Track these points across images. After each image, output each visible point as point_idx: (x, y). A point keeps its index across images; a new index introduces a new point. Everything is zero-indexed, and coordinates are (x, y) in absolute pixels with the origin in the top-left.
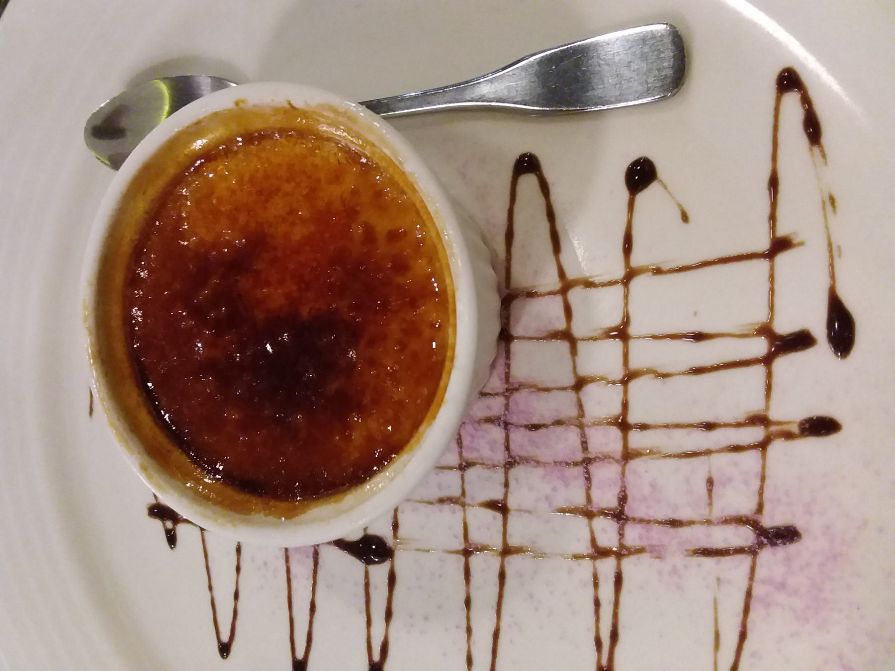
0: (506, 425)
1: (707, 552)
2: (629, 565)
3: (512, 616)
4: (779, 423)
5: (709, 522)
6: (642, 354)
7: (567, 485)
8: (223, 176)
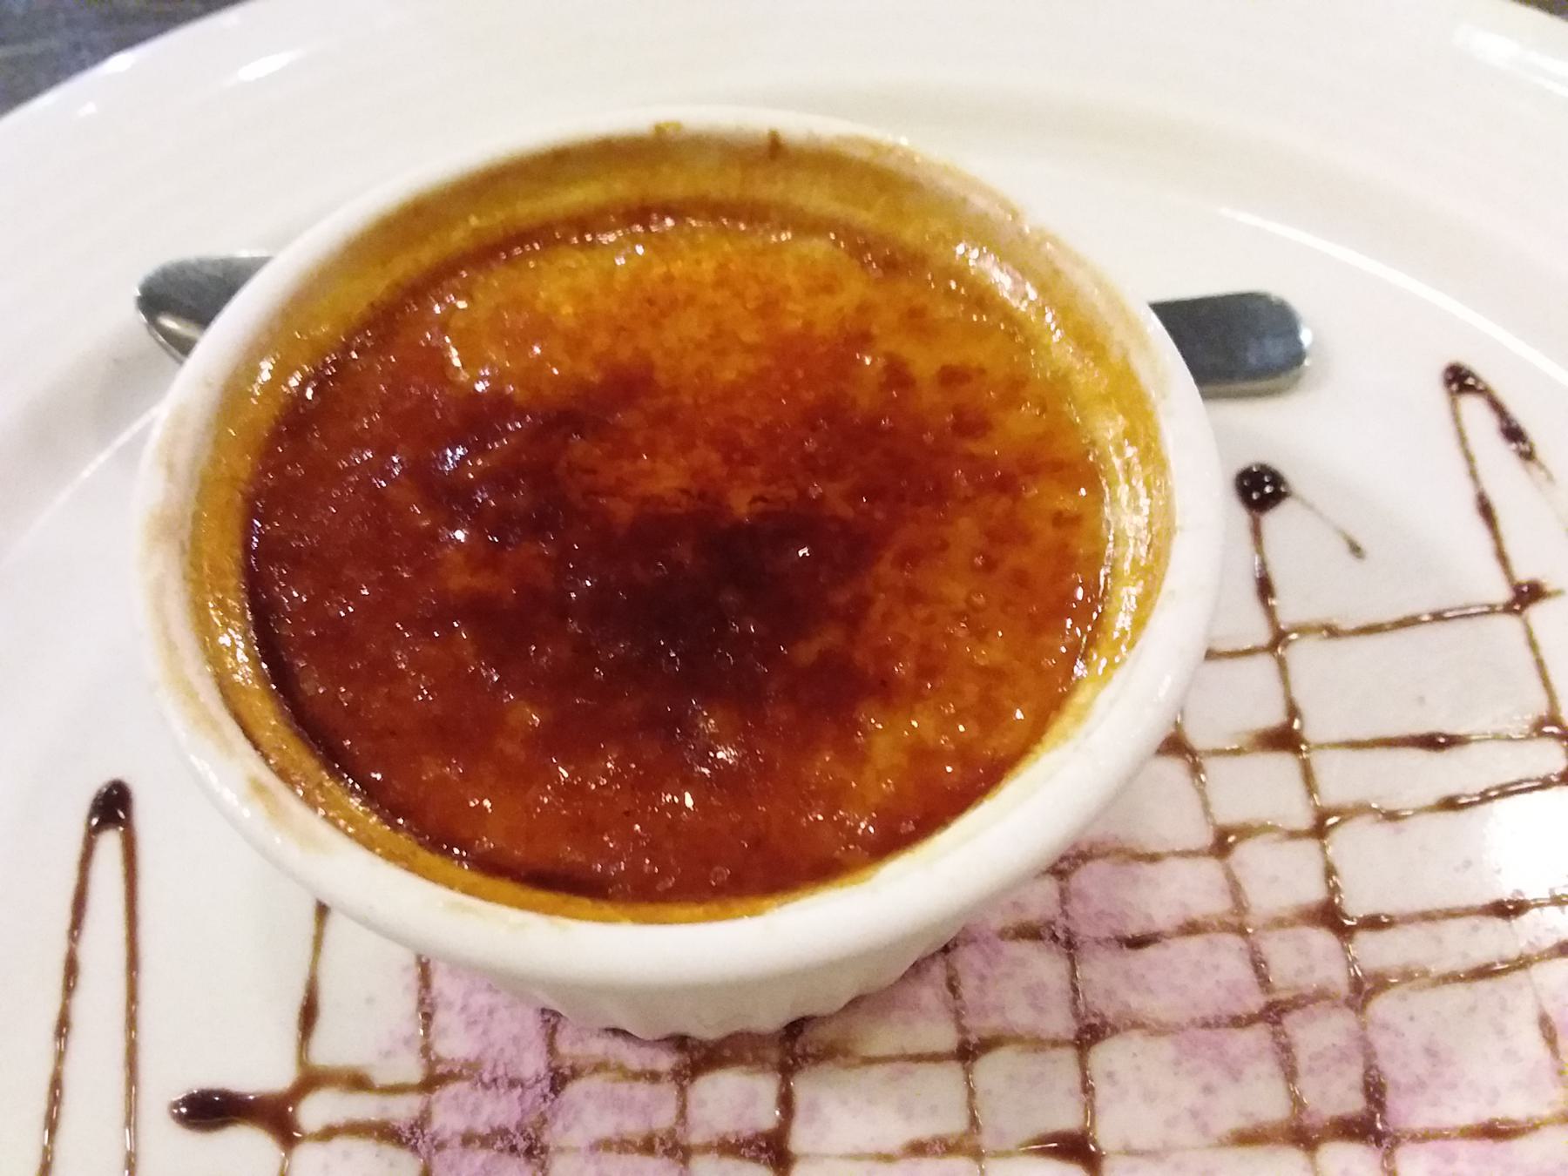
0: (1070, 946)
6: (1341, 778)
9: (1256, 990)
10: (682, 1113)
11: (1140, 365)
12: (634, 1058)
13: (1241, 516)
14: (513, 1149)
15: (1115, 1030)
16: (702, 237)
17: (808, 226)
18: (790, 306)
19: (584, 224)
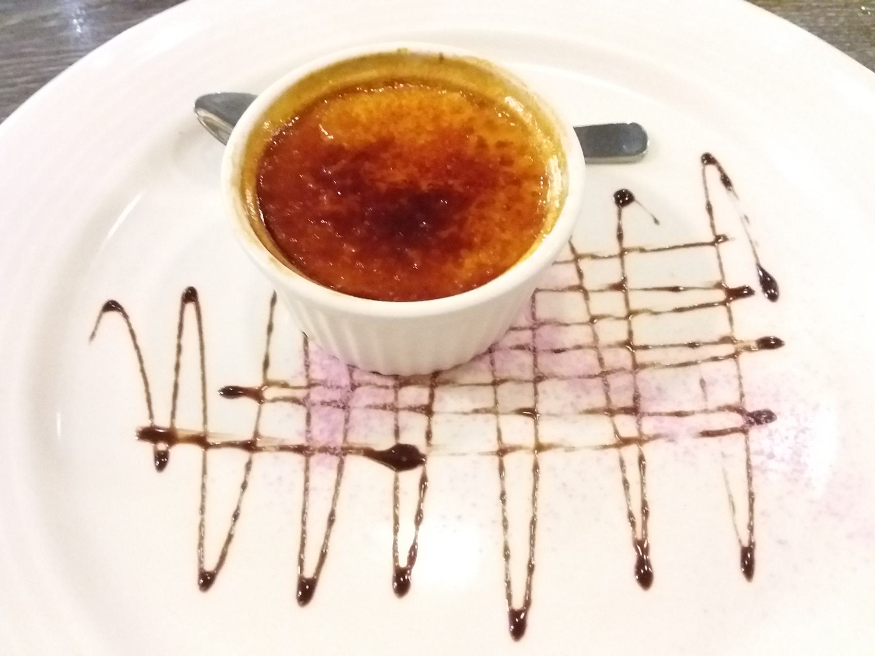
0: (534, 351)
1: (707, 434)
2: (648, 449)
4: (742, 342)
6: (638, 301)
7: (588, 392)
8: (362, 107)
10: (396, 398)
11: (564, 141)
12: (379, 381)
13: (614, 208)
14: (338, 407)
15: (547, 378)
16: (413, 92)
17: (452, 88)
18: (445, 118)
19: (369, 85)
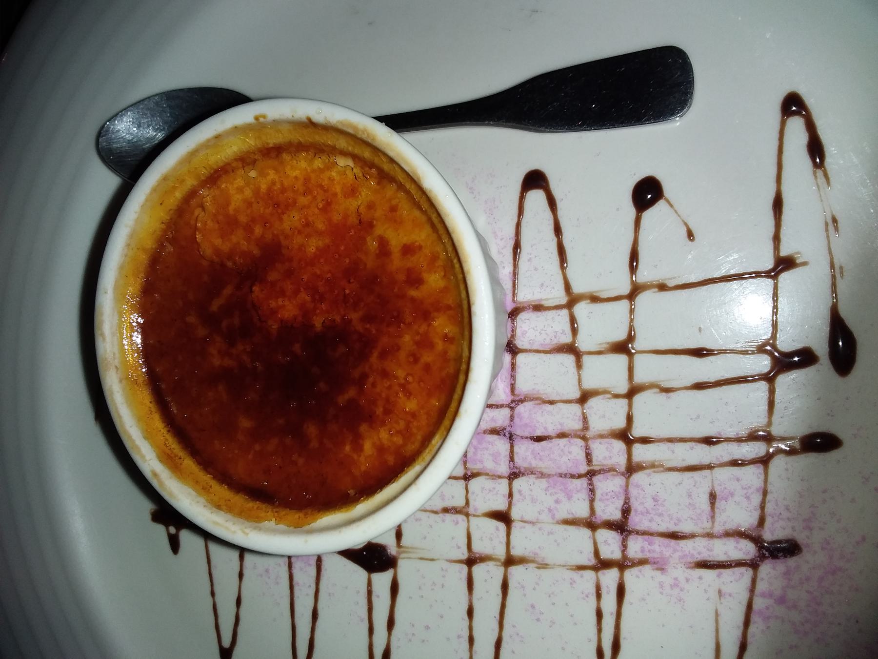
1: (704, 565)
3: (514, 626)
5: (710, 536)
6: (648, 369)
9: (584, 462)
15: (523, 474)
